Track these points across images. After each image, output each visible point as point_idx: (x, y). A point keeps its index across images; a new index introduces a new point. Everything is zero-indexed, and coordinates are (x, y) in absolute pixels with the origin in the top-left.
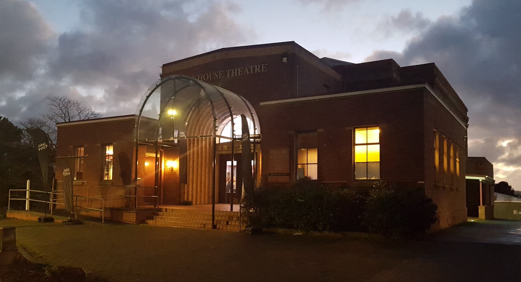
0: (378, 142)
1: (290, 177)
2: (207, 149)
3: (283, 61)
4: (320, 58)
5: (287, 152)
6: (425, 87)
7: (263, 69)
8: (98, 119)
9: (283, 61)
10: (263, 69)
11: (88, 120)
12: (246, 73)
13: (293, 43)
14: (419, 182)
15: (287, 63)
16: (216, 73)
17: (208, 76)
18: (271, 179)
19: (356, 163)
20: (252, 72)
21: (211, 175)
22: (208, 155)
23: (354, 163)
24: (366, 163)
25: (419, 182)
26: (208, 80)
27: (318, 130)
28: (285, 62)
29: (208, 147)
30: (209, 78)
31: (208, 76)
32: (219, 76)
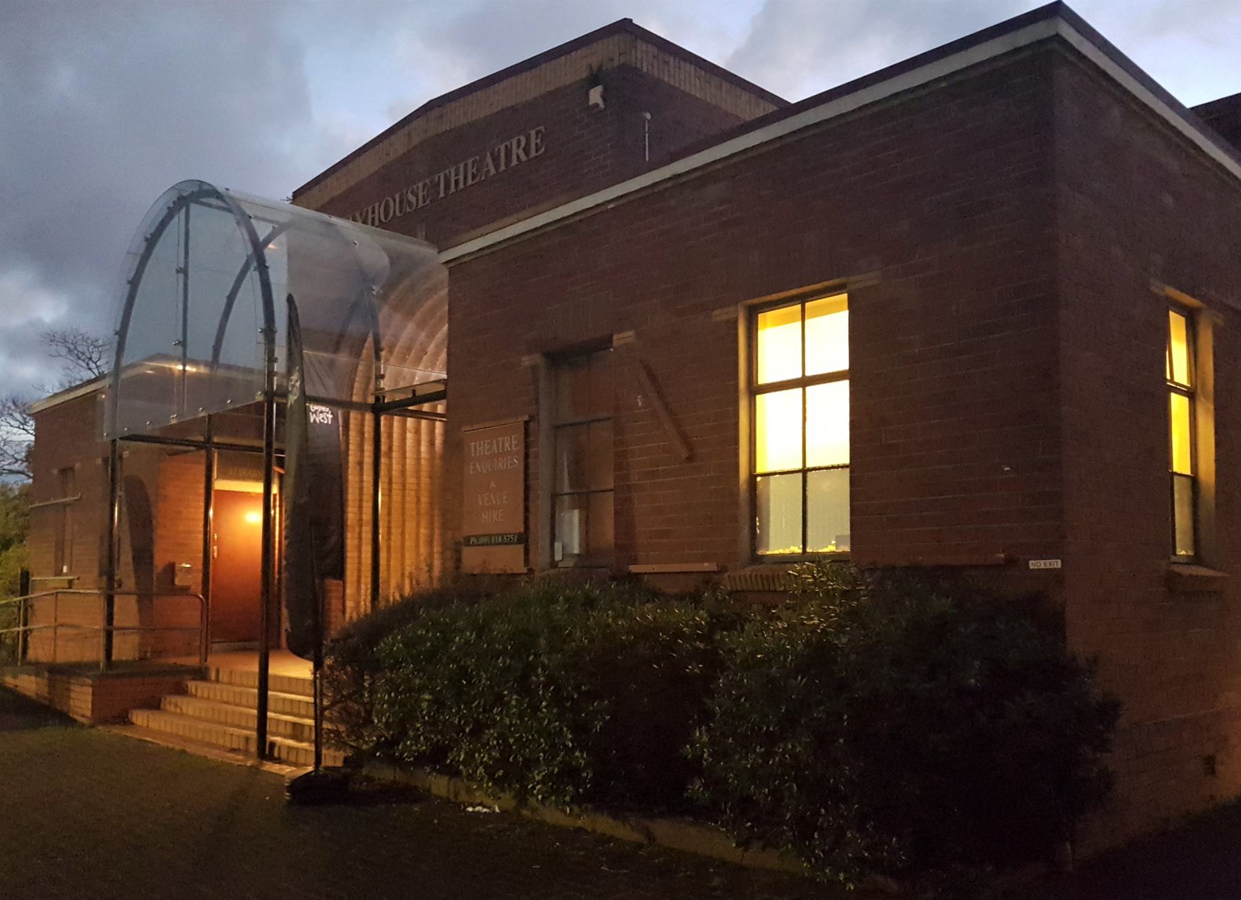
0: (844, 365)
1: (527, 552)
2: (423, 462)
3: (592, 102)
4: (793, 101)
5: (516, 445)
6: (1058, 38)
7: (533, 147)
8: (78, 387)
9: (592, 102)
10: (533, 147)
11: (71, 389)
12: (488, 171)
13: (625, 19)
14: (1034, 564)
15: (602, 105)
16: (411, 192)
17: (392, 204)
18: (472, 559)
19: (759, 479)
20: (503, 168)
21: (436, 549)
22: (425, 480)
23: (753, 477)
24: (800, 475)
25: (1034, 564)
26: (392, 218)
27: (615, 337)
28: (597, 105)
29: (423, 455)
30: (395, 211)
31: (392, 204)
32: (417, 200)
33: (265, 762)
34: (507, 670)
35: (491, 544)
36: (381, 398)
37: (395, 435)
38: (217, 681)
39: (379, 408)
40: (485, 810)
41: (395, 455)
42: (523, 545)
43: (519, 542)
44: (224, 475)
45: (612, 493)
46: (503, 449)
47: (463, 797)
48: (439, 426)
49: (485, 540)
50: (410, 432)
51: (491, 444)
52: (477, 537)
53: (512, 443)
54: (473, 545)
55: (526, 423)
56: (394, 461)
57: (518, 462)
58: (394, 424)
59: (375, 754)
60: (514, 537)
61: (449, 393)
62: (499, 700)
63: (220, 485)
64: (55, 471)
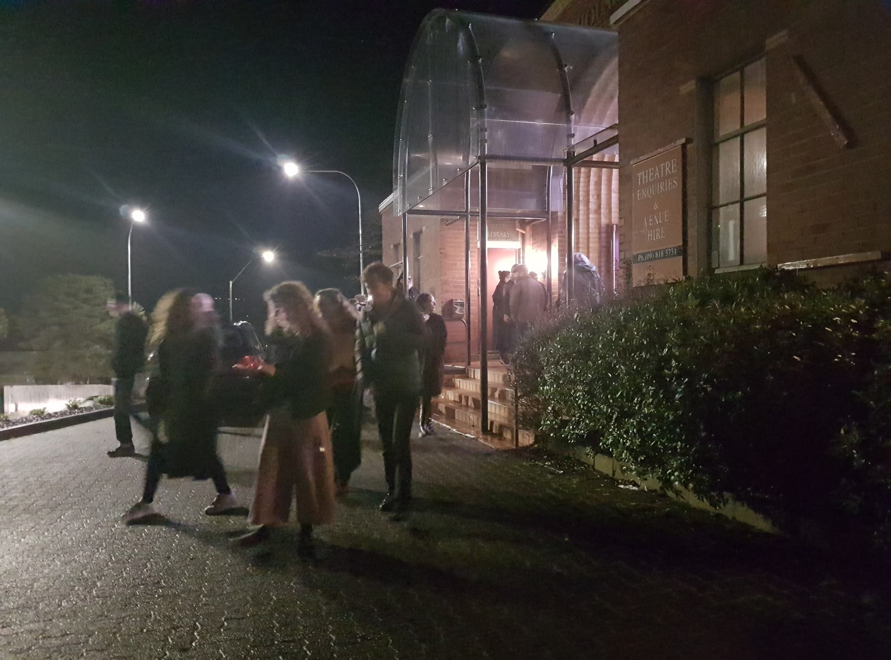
33: (147, 463)
34: (643, 363)
35: (655, 259)
36: (572, 153)
37: (603, 197)
38: (474, 378)
39: (571, 161)
40: (634, 488)
41: (603, 211)
42: (681, 257)
43: (678, 254)
44: (490, 239)
45: (765, 198)
46: (664, 174)
47: (618, 475)
48: (615, 172)
49: (650, 256)
50: (615, 192)
51: (654, 171)
52: (644, 255)
53: (672, 167)
54: (641, 261)
55: (684, 146)
56: (602, 216)
57: (677, 183)
58: (579, 174)
59: (550, 435)
60: (674, 250)
61: (621, 139)
62: (638, 391)
63: (489, 244)
64: (392, 246)
